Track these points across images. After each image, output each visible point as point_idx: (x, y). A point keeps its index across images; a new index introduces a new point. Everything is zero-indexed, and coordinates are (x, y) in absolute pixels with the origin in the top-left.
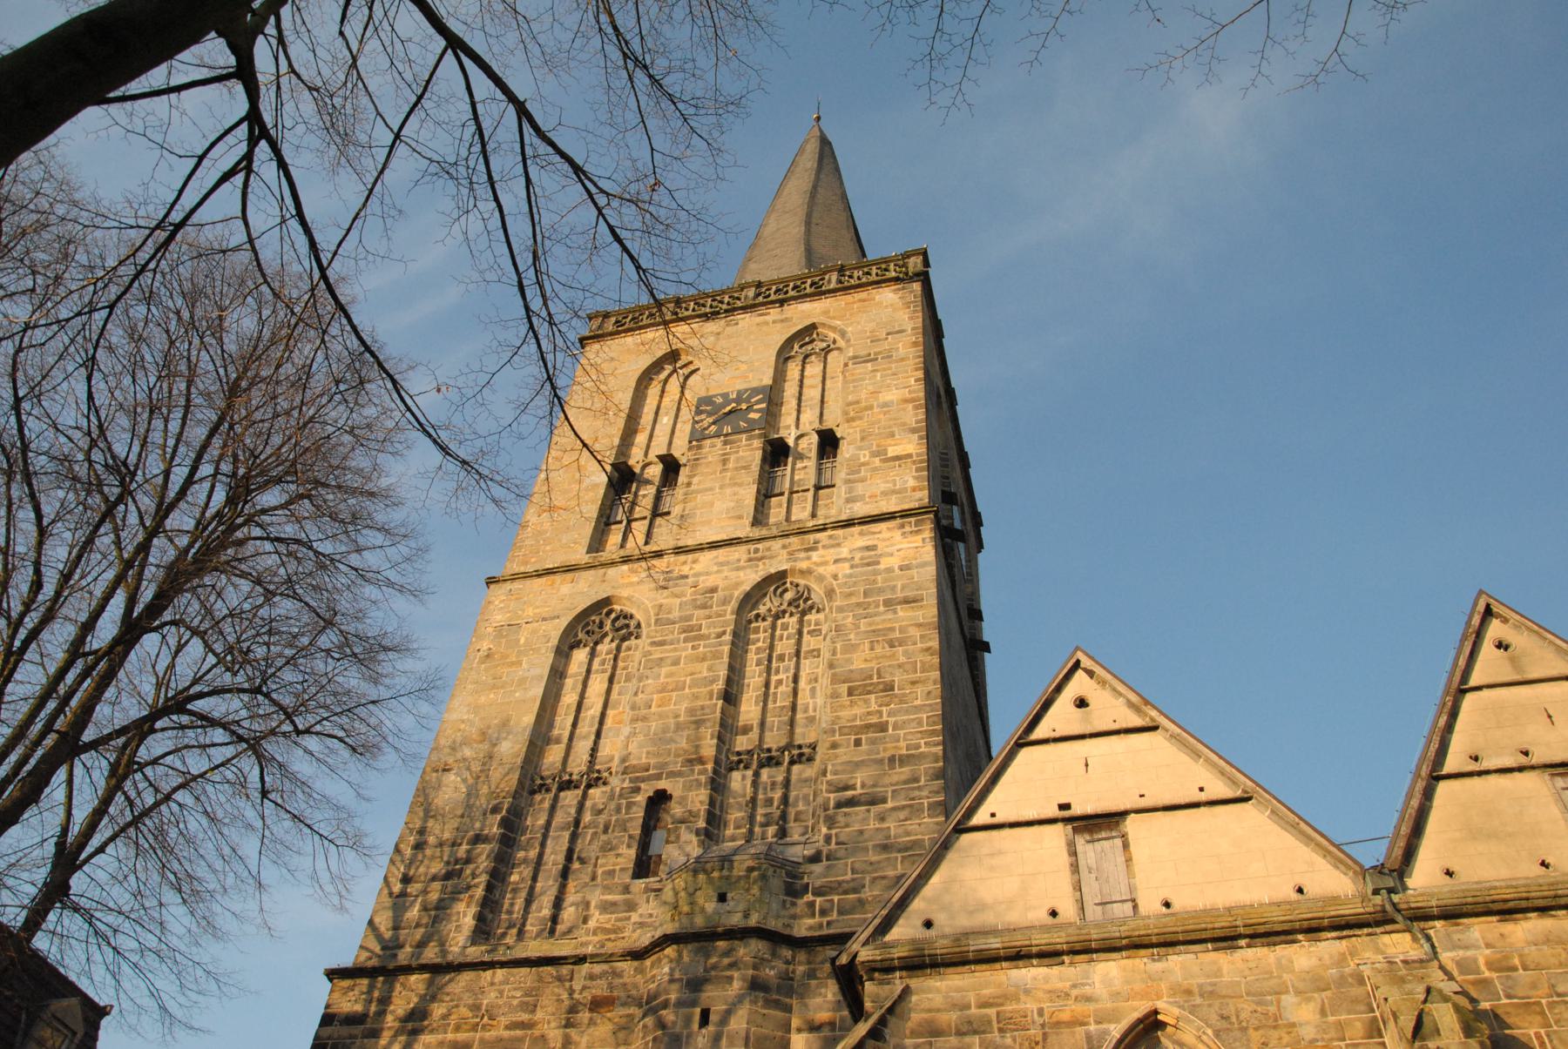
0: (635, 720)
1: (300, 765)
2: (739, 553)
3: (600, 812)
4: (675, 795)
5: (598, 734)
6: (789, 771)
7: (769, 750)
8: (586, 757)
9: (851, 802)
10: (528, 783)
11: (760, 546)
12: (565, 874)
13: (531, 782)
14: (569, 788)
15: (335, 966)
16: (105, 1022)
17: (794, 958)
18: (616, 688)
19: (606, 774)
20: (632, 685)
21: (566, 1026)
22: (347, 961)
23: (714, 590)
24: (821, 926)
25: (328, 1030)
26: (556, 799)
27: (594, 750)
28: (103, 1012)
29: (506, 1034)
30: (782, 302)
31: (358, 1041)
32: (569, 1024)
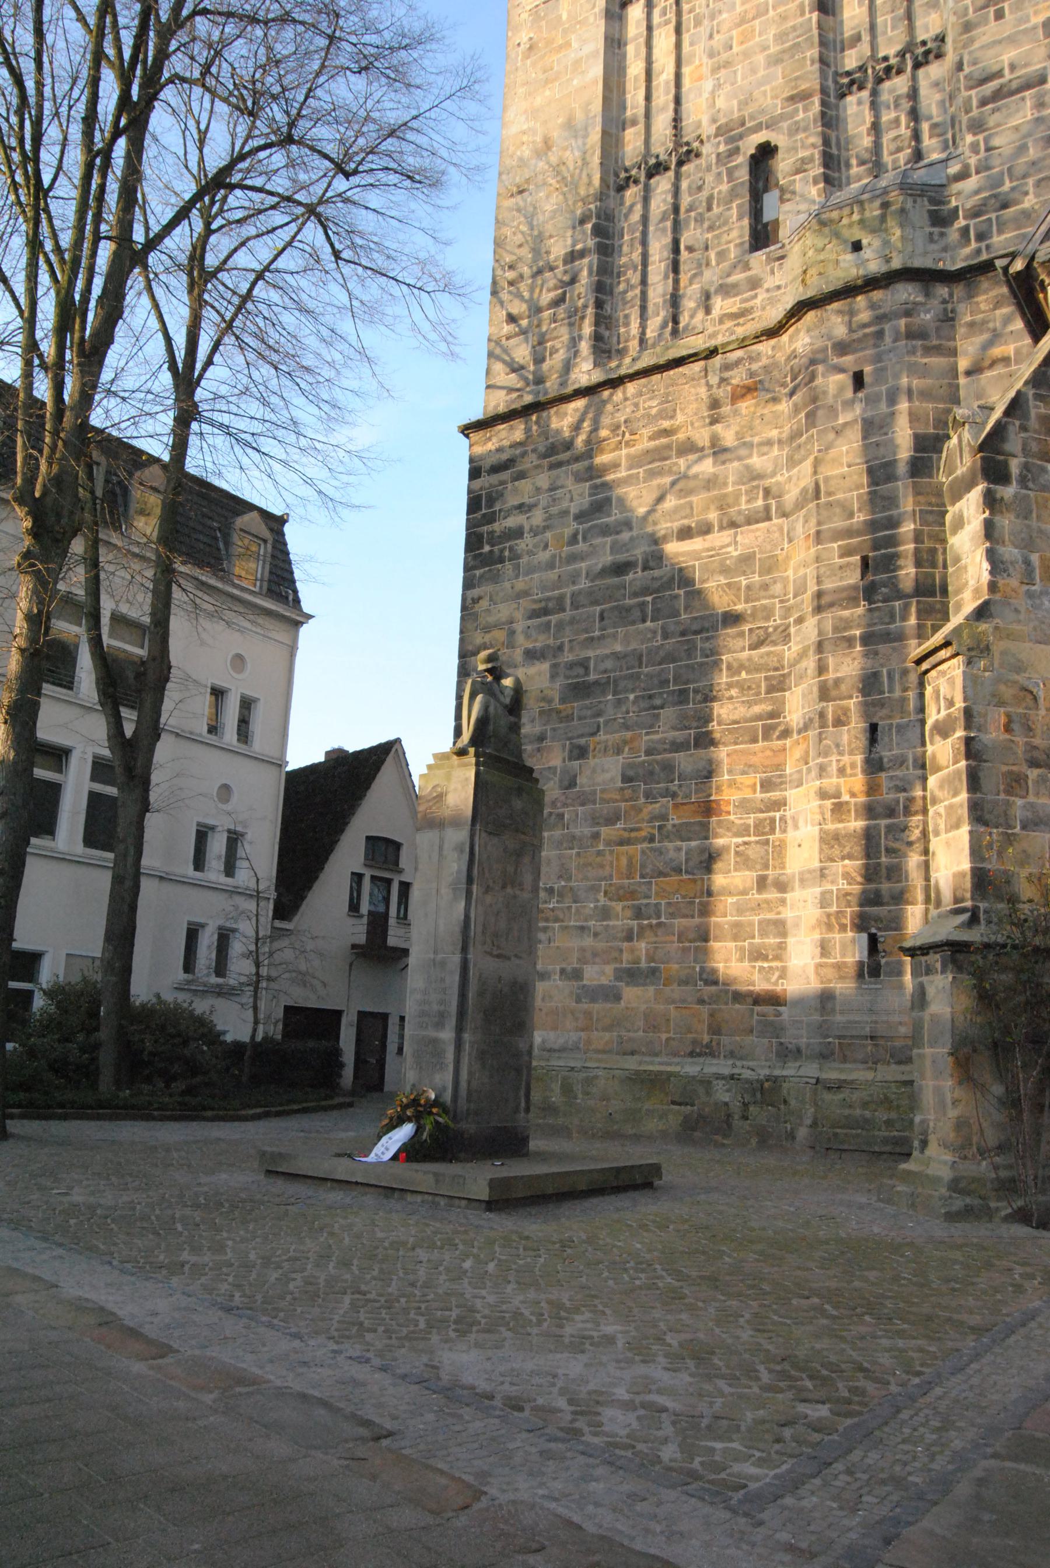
0: (716, 69)
1: (365, 221)
3: (700, 189)
4: (779, 144)
5: (678, 101)
6: (914, 78)
7: (886, 59)
8: (670, 131)
9: (998, 95)
10: (612, 179)
12: (675, 267)
13: (617, 180)
14: (658, 173)
15: (466, 422)
16: (287, 529)
17: (951, 295)
18: (686, 38)
19: (696, 145)
20: (703, 30)
21: (712, 423)
22: (476, 413)
24: (978, 251)
25: (478, 483)
26: (647, 189)
27: (677, 120)
28: (282, 521)
29: (652, 444)
31: (509, 486)
32: (714, 421)
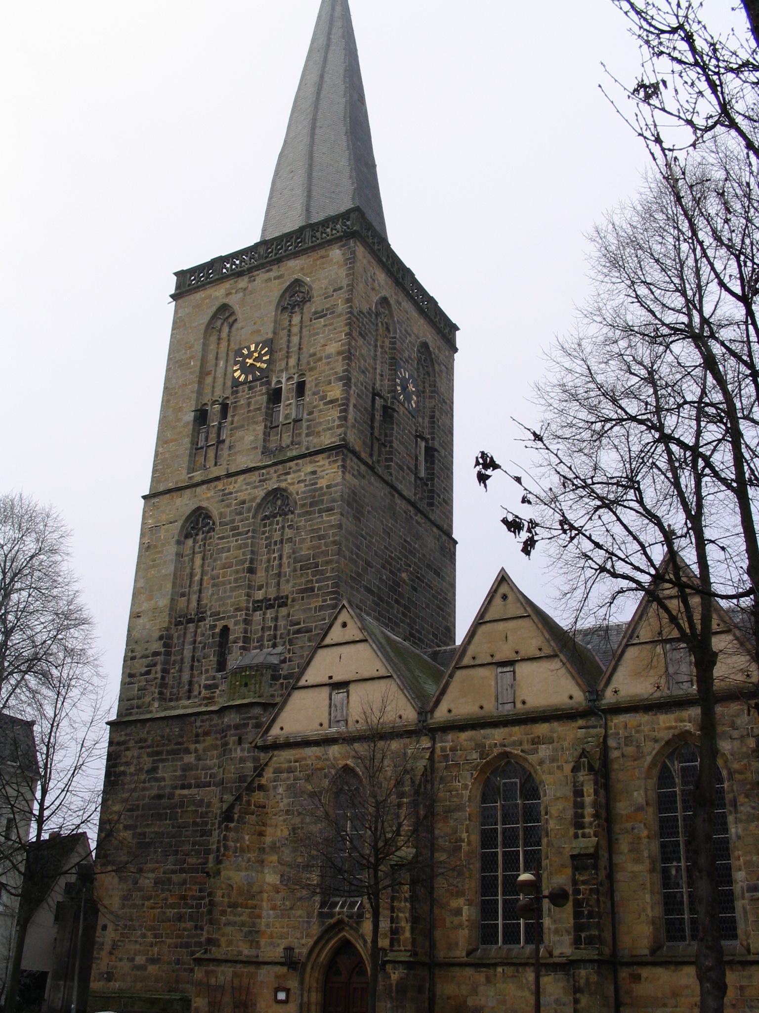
2: (254, 477)
6: (277, 611)
9: (298, 631)
11: (264, 471)
23: (244, 502)
30: (279, 261)
